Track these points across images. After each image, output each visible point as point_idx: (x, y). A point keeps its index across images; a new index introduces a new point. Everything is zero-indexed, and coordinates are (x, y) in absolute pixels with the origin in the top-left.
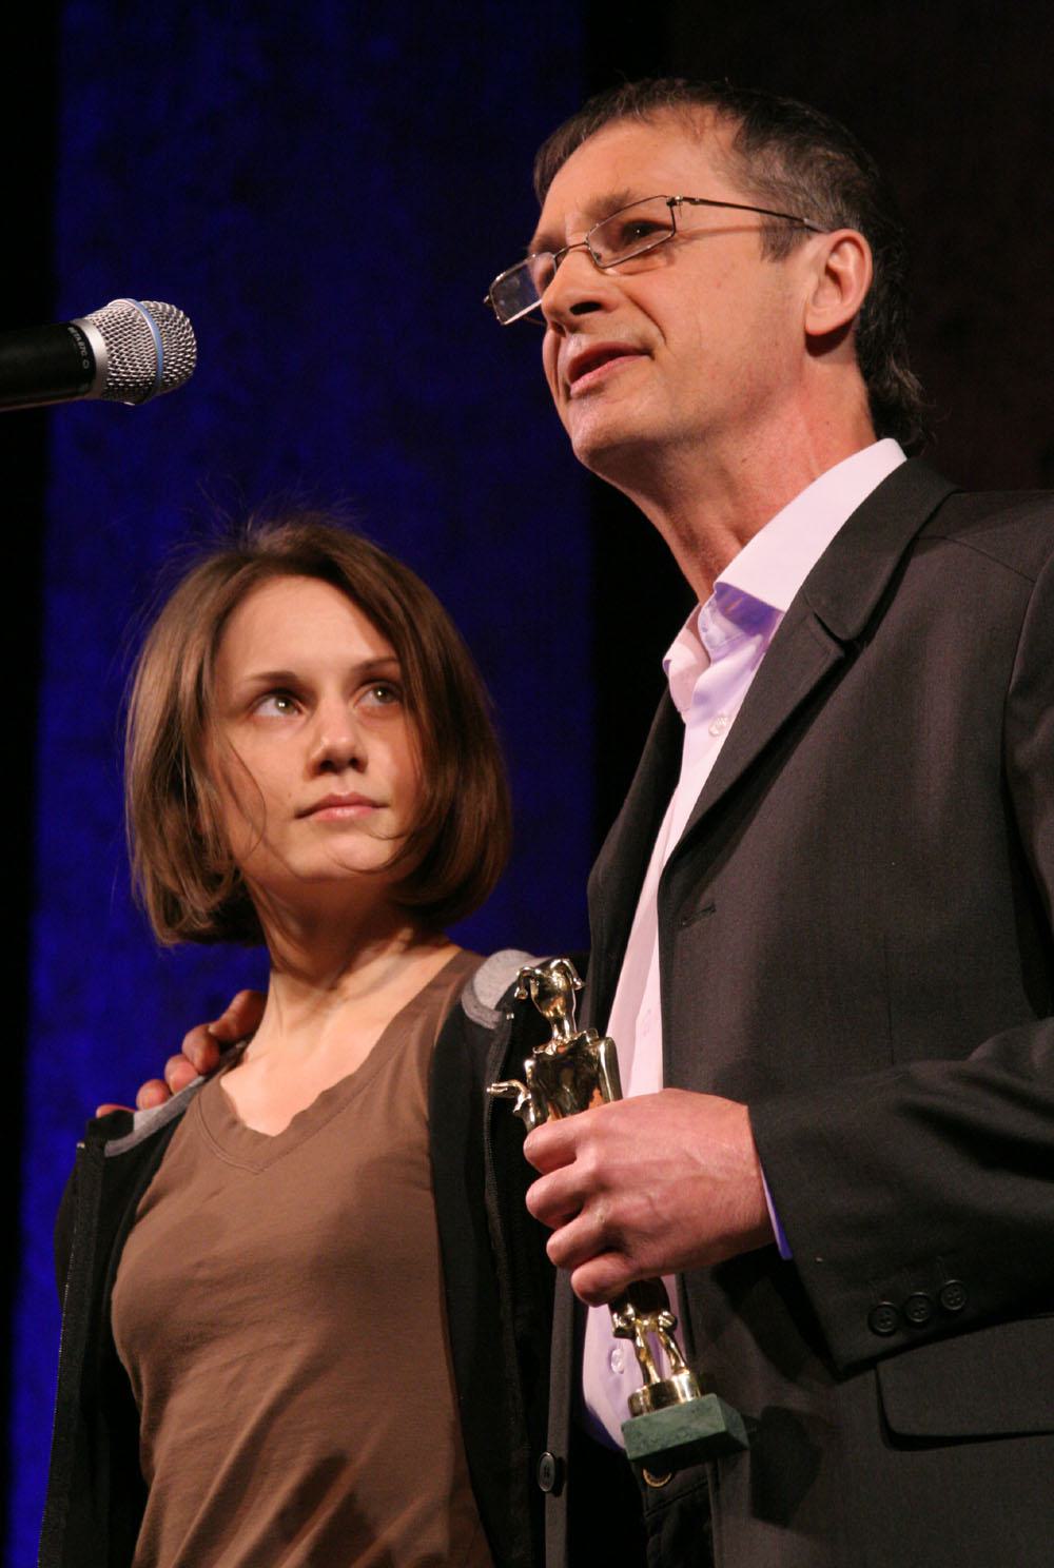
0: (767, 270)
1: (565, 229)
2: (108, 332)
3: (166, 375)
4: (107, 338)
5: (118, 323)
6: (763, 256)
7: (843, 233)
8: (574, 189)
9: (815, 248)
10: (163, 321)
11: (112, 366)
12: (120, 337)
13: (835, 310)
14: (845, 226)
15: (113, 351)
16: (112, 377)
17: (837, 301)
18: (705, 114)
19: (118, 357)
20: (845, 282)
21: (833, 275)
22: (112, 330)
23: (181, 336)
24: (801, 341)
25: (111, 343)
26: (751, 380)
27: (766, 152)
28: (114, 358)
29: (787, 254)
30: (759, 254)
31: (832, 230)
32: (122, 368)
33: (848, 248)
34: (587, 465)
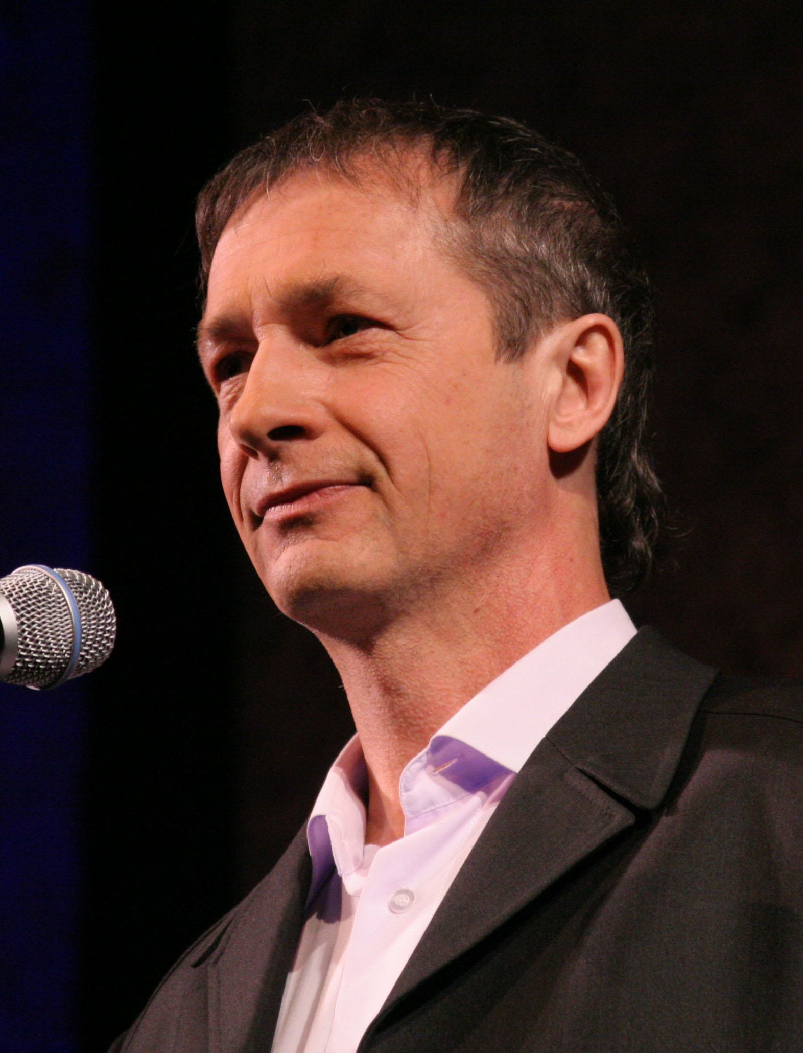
0: (503, 372)
1: (252, 313)
2: (19, 604)
3: (82, 656)
4: (18, 611)
5: (31, 593)
6: (497, 359)
7: (591, 320)
8: (251, 255)
9: (556, 339)
10: (81, 593)
11: (22, 643)
12: (33, 610)
13: (582, 421)
14: (588, 309)
15: (24, 627)
16: (21, 656)
17: (581, 405)
18: (416, 159)
19: (30, 633)
20: (592, 380)
21: (576, 372)
22: (24, 602)
23: (92, 608)
24: (543, 458)
25: (23, 616)
26: (486, 517)
27: (496, 216)
28: (26, 634)
29: (522, 353)
30: (493, 355)
31: (574, 317)
32: (33, 646)
33: (598, 342)
34: (289, 616)
